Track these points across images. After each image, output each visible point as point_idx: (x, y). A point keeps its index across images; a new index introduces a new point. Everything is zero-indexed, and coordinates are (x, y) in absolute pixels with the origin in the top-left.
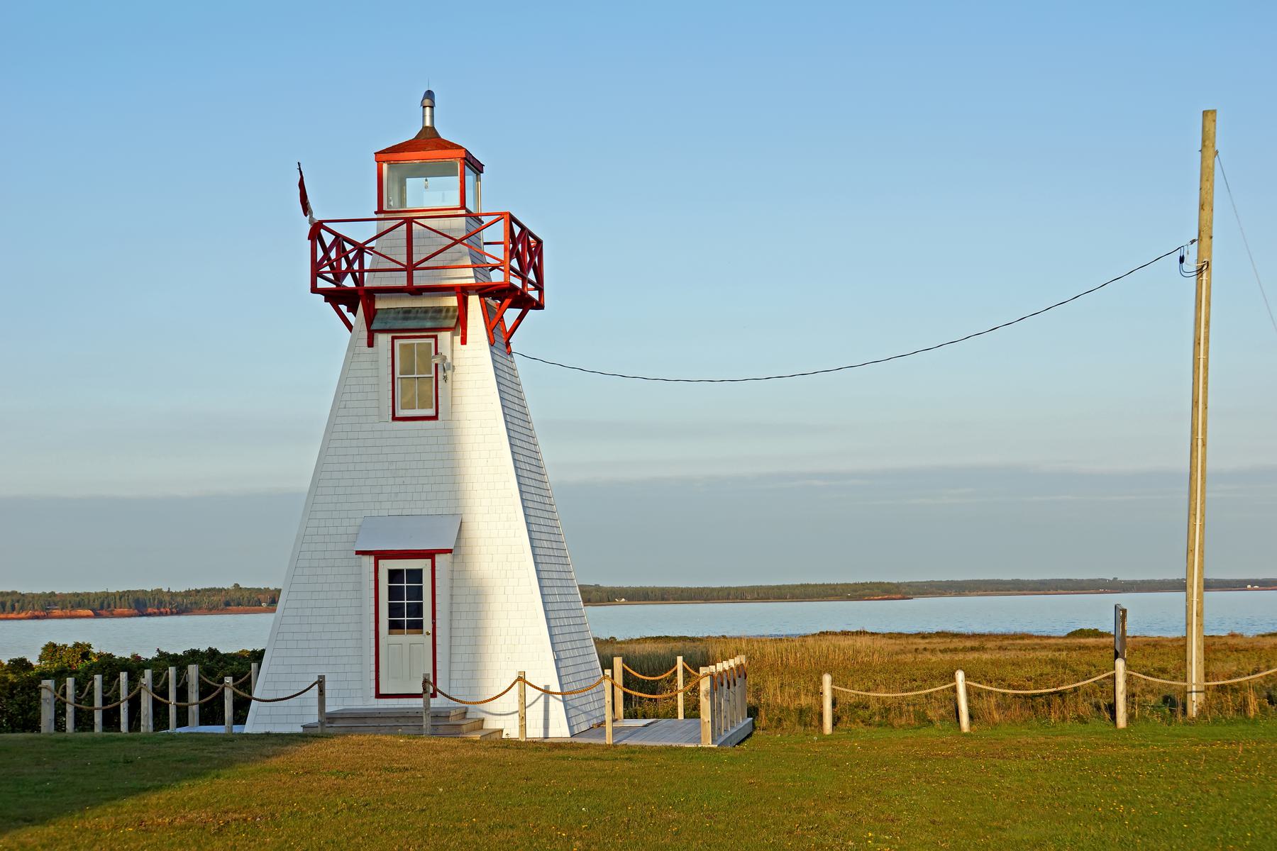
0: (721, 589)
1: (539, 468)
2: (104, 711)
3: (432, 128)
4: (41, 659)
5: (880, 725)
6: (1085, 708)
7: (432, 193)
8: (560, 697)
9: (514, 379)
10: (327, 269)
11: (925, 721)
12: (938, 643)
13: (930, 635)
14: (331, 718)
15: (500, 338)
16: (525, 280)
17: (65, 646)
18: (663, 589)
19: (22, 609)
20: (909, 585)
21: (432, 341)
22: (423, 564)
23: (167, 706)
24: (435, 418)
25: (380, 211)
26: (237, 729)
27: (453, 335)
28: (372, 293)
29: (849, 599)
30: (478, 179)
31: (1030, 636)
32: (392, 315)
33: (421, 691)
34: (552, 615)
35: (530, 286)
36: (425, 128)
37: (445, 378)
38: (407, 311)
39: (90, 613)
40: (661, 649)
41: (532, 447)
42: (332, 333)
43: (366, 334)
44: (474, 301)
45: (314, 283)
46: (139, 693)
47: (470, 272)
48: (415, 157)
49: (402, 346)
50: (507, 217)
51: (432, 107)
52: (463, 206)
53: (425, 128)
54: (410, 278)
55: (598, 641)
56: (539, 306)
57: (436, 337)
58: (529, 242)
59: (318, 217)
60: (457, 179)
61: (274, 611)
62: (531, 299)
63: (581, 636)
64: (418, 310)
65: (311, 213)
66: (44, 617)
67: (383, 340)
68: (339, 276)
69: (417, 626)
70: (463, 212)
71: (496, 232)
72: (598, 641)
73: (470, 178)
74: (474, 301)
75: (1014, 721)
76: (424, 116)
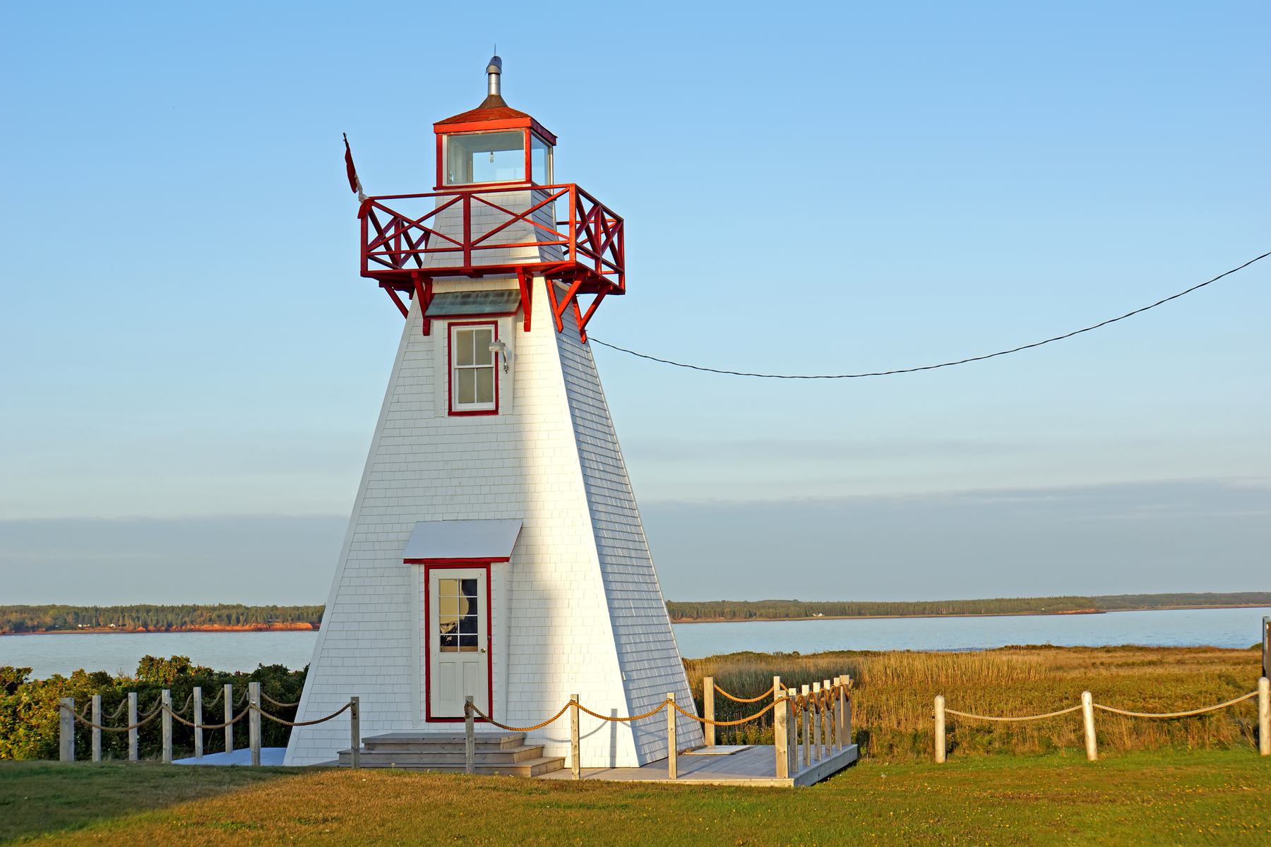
0: (917, 604)
1: (616, 469)
3: (499, 97)
4: (139, 673)
5: (1000, 752)
6: (1228, 730)
7: (498, 167)
9: (589, 371)
10: (382, 249)
11: (1050, 748)
12: (1119, 657)
13: (1115, 649)
14: (371, 744)
15: (572, 328)
17: (162, 660)
18: (860, 604)
19: (246, 621)
20: (1103, 599)
21: (492, 327)
22: (478, 574)
24: (495, 412)
25: (439, 186)
26: (269, 757)
29: (1044, 613)
30: (550, 152)
31: (1213, 650)
32: (449, 300)
33: (463, 715)
34: (622, 631)
35: (605, 268)
36: (490, 96)
37: (506, 369)
38: (466, 295)
39: (309, 626)
40: (762, 667)
41: (610, 446)
42: (384, 319)
43: (421, 320)
44: (539, 284)
46: (248, 714)
47: (535, 251)
49: (459, 333)
50: (572, 189)
51: (498, 74)
52: (529, 179)
53: (490, 96)
54: (467, 258)
55: (689, 665)
56: (619, 290)
57: (496, 323)
58: (604, 222)
59: (368, 193)
60: (522, 153)
62: (608, 283)
63: (664, 654)
64: (477, 294)
65: (361, 189)
67: (439, 327)
69: (471, 643)
71: (562, 209)
72: (689, 665)
73: (539, 153)
74: (539, 284)
75: (1147, 749)
76: (489, 84)
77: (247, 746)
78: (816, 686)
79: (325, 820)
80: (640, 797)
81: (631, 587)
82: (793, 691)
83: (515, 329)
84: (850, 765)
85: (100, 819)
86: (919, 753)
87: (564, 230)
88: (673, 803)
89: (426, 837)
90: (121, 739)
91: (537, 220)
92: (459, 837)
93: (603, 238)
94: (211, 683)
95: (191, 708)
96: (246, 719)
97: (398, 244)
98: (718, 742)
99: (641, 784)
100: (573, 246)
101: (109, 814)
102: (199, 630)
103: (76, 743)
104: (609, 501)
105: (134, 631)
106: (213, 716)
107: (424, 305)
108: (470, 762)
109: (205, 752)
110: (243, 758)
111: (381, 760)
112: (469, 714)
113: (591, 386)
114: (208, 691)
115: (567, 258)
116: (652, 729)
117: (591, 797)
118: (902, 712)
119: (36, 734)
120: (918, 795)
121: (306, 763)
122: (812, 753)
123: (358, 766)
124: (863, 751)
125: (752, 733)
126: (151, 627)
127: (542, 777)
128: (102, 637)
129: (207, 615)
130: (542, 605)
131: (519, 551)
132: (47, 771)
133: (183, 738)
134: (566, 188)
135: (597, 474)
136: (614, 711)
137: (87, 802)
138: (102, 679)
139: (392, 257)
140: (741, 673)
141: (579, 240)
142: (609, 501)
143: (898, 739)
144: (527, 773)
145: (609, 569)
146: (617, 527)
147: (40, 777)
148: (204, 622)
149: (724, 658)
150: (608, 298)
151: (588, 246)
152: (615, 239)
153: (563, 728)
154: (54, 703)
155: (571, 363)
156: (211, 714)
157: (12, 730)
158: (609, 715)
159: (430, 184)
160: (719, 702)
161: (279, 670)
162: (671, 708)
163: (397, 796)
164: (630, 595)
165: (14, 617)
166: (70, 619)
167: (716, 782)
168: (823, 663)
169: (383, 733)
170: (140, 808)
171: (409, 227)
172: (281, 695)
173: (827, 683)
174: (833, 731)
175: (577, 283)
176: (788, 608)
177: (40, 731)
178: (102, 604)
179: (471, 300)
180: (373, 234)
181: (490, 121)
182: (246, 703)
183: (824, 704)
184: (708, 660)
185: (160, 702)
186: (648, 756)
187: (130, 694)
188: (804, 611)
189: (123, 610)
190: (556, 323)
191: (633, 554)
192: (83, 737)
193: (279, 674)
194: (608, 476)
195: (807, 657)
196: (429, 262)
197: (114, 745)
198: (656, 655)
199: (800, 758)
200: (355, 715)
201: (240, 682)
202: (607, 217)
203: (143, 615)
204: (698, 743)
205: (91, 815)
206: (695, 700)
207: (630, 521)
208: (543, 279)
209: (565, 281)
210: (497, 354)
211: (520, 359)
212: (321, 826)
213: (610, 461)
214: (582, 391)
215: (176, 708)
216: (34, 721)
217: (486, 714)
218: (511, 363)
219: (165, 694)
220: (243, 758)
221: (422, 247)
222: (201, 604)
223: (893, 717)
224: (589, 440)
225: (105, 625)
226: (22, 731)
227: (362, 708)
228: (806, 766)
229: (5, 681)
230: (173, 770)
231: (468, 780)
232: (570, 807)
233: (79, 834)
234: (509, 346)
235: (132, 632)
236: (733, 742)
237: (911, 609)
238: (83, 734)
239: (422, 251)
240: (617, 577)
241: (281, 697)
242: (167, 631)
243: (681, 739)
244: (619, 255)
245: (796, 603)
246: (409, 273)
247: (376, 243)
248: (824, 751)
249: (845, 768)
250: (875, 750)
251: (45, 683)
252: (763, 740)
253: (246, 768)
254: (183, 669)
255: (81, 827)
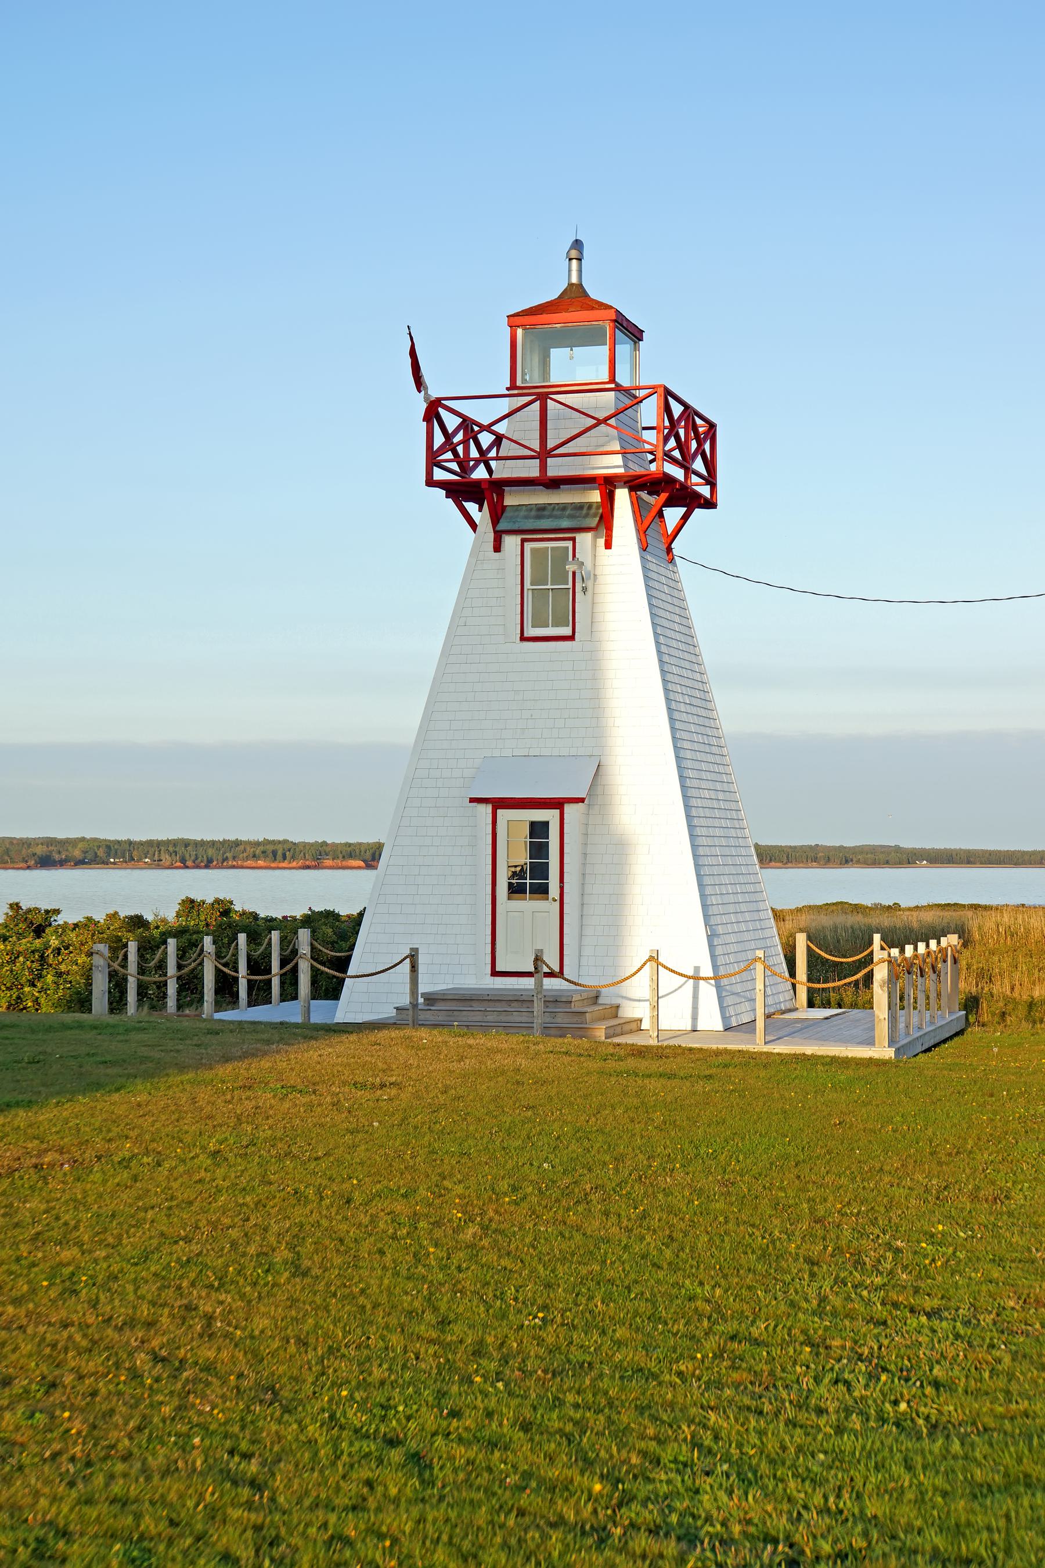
0: (1034, 853)
1: (704, 701)
2: (179, 978)
4: (178, 915)
7: (578, 365)
8: (713, 982)
9: (676, 593)
10: (449, 455)
14: (431, 999)
15: (658, 545)
16: (688, 471)
18: (969, 851)
19: (293, 858)
21: (570, 544)
22: (550, 816)
23: (236, 980)
24: (571, 638)
25: (513, 386)
26: (321, 1012)
27: (596, 537)
28: (498, 486)
30: (636, 348)
32: (522, 513)
33: (532, 969)
34: (707, 880)
35: (695, 479)
36: (571, 285)
37: (585, 590)
38: (542, 508)
39: (362, 864)
40: (858, 919)
41: (698, 677)
42: (451, 534)
43: (492, 535)
44: (622, 496)
45: (429, 474)
46: (297, 964)
47: (618, 460)
48: (557, 321)
49: (533, 550)
50: (661, 391)
51: (580, 260)
52: (612, 380)
53: (571, 285)
54: (543, 467)
55: (779, 916)
57: (574, 540)
58: (695, 427)
59: (435, 393)
60: (605, 350)
61: (375, 868)
62: (699, 496)
63: (753, 907)
65: (426, 389)
66: (316, 867)
67: (511, 542)
68: (465, 466)
69: (542, 891)
70: (613, 386)
71: (649, 412)
72: (779, 916)
73: (624, 349)
74: (622, 496)
76: (570, 271)
77: (295, 998)
78: (922, 946)
79: (383, 1086)
80: (726, 1066)
81: (718, 832)
82: (895, 952)
83: (595, 546)
84: (957, 1034)
85: (138, 1081)
86: (1034, 1022)
87: (651, 436)
88: (763, 1074)
89: (492, 1107)
90: (159, 987)
91: (621, 425)
92: (528, 1108)
93: (694, 445)
94: (257, 928)
95: (235, 955)
96: (295, 970)
97: (467, 450)
98: (811, 1004)
99: (726, 1051)
100: (660, 454)
101: (148, 1075)
102: (242, 867)
103: (110, 992)
104: (695, 737)
105: (171, 867)
106: (258, 966)
107: (495, 519)
108: (538, 1021)
109: (251, 1003)
110: (290, 1012)
111: (441, 1018)
112: (538, 969)
113: (677, 610)
114: (254, 938)
115: (653, 467)
116: (738, 989)
117: (671, 1065)
118: (1017, 975)
119: (65, 981)
120: (1034, 1073)
121: (359, 1019)
122: (915, 1020)
123: (417, 1024)
124: (972, 1019)
125: (848, 996)
126: (189, 863)
127: (617, 1040)
128: (136, 873)
129: (250, 850)
130: (620, 851)
131: (593, 795)
132: (80, 1026)
133: (226, 988)
134: (654, 389)
135: (682, 707)
136: (697, 969)
137: (124, 1061)
138: (137, 922)
139: (460, 464)
140: (836, 928)
141: (667, 448)
142: (695, 737)
143: (1010, 1006)
144: (600, 1034)
145: (694, 812)
146: (704, 766)
147: (73, 1032)
148: (247, 858)
149: (818, 909)
150: (697, 512)
151: (676, 454)
152: (707, 447)
153: (639, 987)
154: (86, 948)
155: (656, 585)
156: (256, 962)
157: (40, 977)
158: (691, 973)
159: (502, 385)
160: (813, 960)
161: (330, 916)
162: (759, 967)
163: (461, 1059)
164: (717, 841)
165: (40, 850)
166: (101, 853)
167: (809, 1050)
168: (929, 917)
169: (444, 987)
170: (182, 1068)
171: (479, 432)
172: (333, 943)
173: (933, 943)
174: (939, 995)
175: (664, 496)
176: (889, 853)
177: (69, 978)
178: (137, 837)
179: (546, 513)
180: (439, 439)
181: (571, 313)
182: (295, 952)
183: (930, 967)
184: (799, 910)
185: (202, 950)
186: (733, 1019)
187: (170, 940)
188: (907, 858)
189: (159, 844)
190: (640, 540)
191: (721, 796)
192: (117, 985)
193: (331, 919)
194: (694, 710)
195: (910, 909)
196: (502, 470)
197: (152, 996)
198: (743, 907)
199: (902, 1026)
200: (414, 968)
201: (288, 926)
202: (699, 421)
203: (181, 850)
204: (789, 1006)
205: (129, 1076)
206: (785, 956)
207: (718, 759)
208: (626, 491)
209: (650, 493)
210: (574, 573)
211: (600, 579)
212: (379, 1092)
213: (698, 694)
214: (668, 615)
215: (219, 956)
216: (63, 968)
217: (557, 969)
218: (589, 584)
219: (208, 940)
220: (290, 1012)
221: (493, 453)
222: (244, 838)
223: (1006, 981)
224: (675, 670)
225: (138, 861)
226: (50, 978)
227: (422, 959)
228: (908, 1034)
229: (32, 923)
230: (217, 1027)
231: (538, 1043)
232: (649, 1076)
233: (116, 1097)
234: (588, 565)
235: (169, 868)
236: (826, 1004)
237: (1027, 858)
238: (118, 983)
239: (493, 459)
240: (703, 822)
241: (333, 945)
242: (207, 867)
243: (770, 1001)
244: (710, 465)
245: (897, 849)
246: (479, 482)
247: (442, 450)
248: (928, 1019)
249: (951, 1038)
250: (985, 1018)
251: (76, 926)
252: (860, 1003)
253: (296, 1025)
254: (226, 913)
255: (118, 1090)
